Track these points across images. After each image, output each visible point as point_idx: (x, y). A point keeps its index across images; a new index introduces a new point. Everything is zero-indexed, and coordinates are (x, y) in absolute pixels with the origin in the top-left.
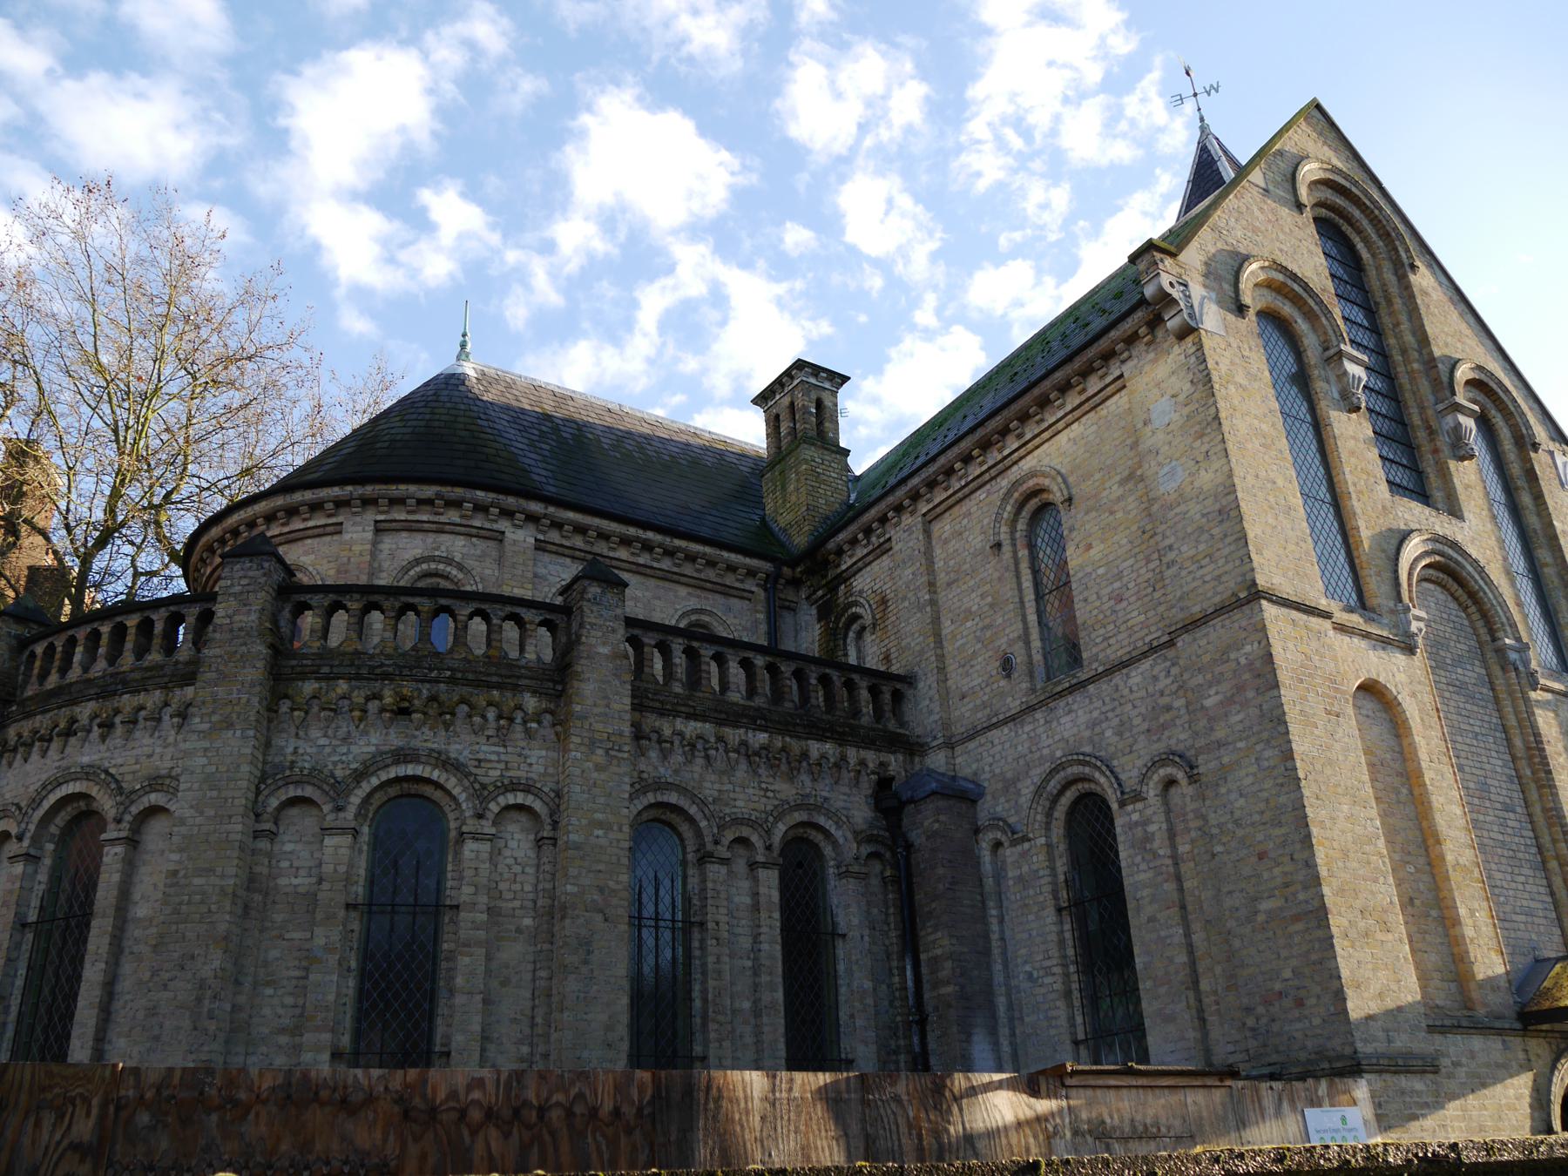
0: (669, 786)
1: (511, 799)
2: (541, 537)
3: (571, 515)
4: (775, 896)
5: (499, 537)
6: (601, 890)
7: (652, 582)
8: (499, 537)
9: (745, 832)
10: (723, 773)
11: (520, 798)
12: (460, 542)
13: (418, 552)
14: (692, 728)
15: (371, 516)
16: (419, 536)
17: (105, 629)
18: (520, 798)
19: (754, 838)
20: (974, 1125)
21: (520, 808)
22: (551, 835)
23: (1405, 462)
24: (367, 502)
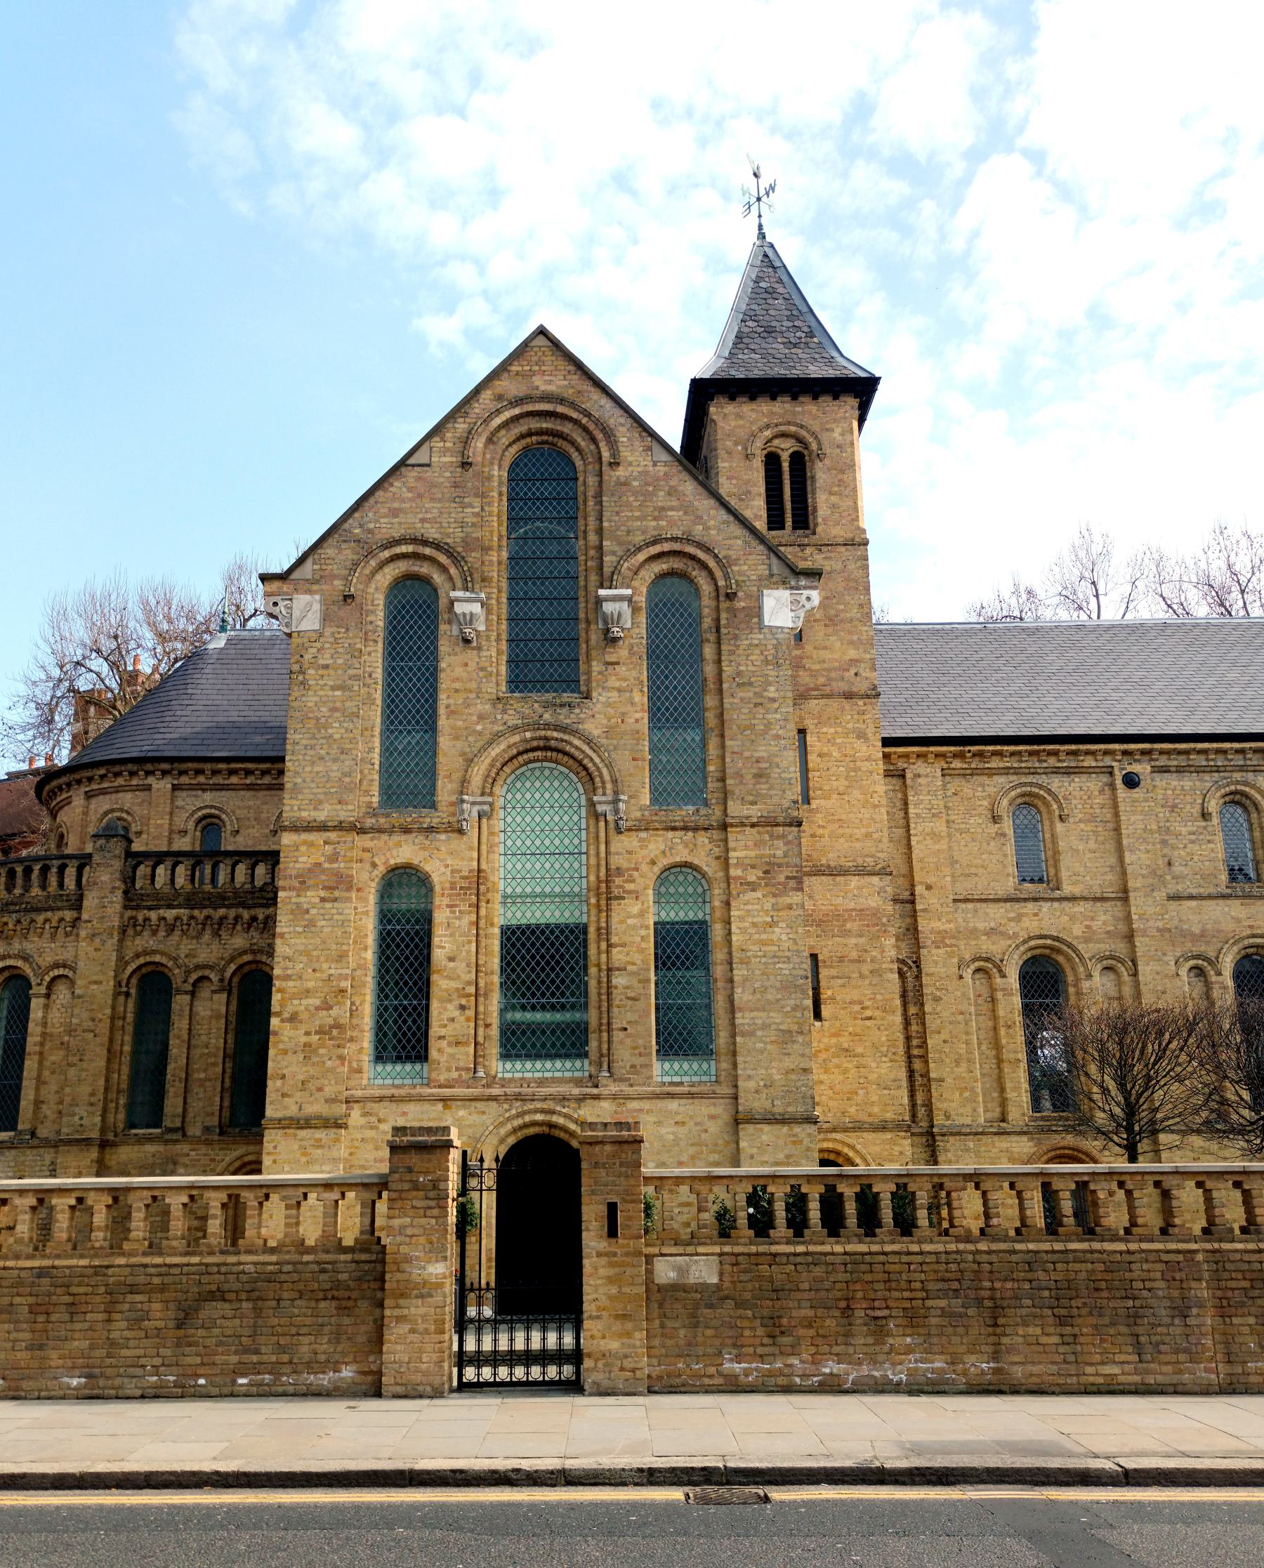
0: (154, 952)
1: (56, 972)
2: (175, 782)
3: (190, 765)
4: (27, 1063)
5: (148, 788)
6: (93, 1020)
7: (261, 793)
8: (148, 788)
9: (207, 972)
10: (193, 938)
11: (62, 971)
12: (129, 795)
13: (107, 807)
14: (170, 914)
15: (84, 789)
16: (108, 797)
17: (37, 868)
18: (62, 971)
19: (212, 976)
20: (1111, 885)
21: (60, 976)
22: (622, 843)
23: (782, 549)
24: (79, 782)
